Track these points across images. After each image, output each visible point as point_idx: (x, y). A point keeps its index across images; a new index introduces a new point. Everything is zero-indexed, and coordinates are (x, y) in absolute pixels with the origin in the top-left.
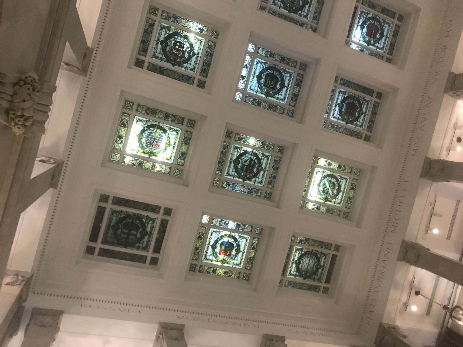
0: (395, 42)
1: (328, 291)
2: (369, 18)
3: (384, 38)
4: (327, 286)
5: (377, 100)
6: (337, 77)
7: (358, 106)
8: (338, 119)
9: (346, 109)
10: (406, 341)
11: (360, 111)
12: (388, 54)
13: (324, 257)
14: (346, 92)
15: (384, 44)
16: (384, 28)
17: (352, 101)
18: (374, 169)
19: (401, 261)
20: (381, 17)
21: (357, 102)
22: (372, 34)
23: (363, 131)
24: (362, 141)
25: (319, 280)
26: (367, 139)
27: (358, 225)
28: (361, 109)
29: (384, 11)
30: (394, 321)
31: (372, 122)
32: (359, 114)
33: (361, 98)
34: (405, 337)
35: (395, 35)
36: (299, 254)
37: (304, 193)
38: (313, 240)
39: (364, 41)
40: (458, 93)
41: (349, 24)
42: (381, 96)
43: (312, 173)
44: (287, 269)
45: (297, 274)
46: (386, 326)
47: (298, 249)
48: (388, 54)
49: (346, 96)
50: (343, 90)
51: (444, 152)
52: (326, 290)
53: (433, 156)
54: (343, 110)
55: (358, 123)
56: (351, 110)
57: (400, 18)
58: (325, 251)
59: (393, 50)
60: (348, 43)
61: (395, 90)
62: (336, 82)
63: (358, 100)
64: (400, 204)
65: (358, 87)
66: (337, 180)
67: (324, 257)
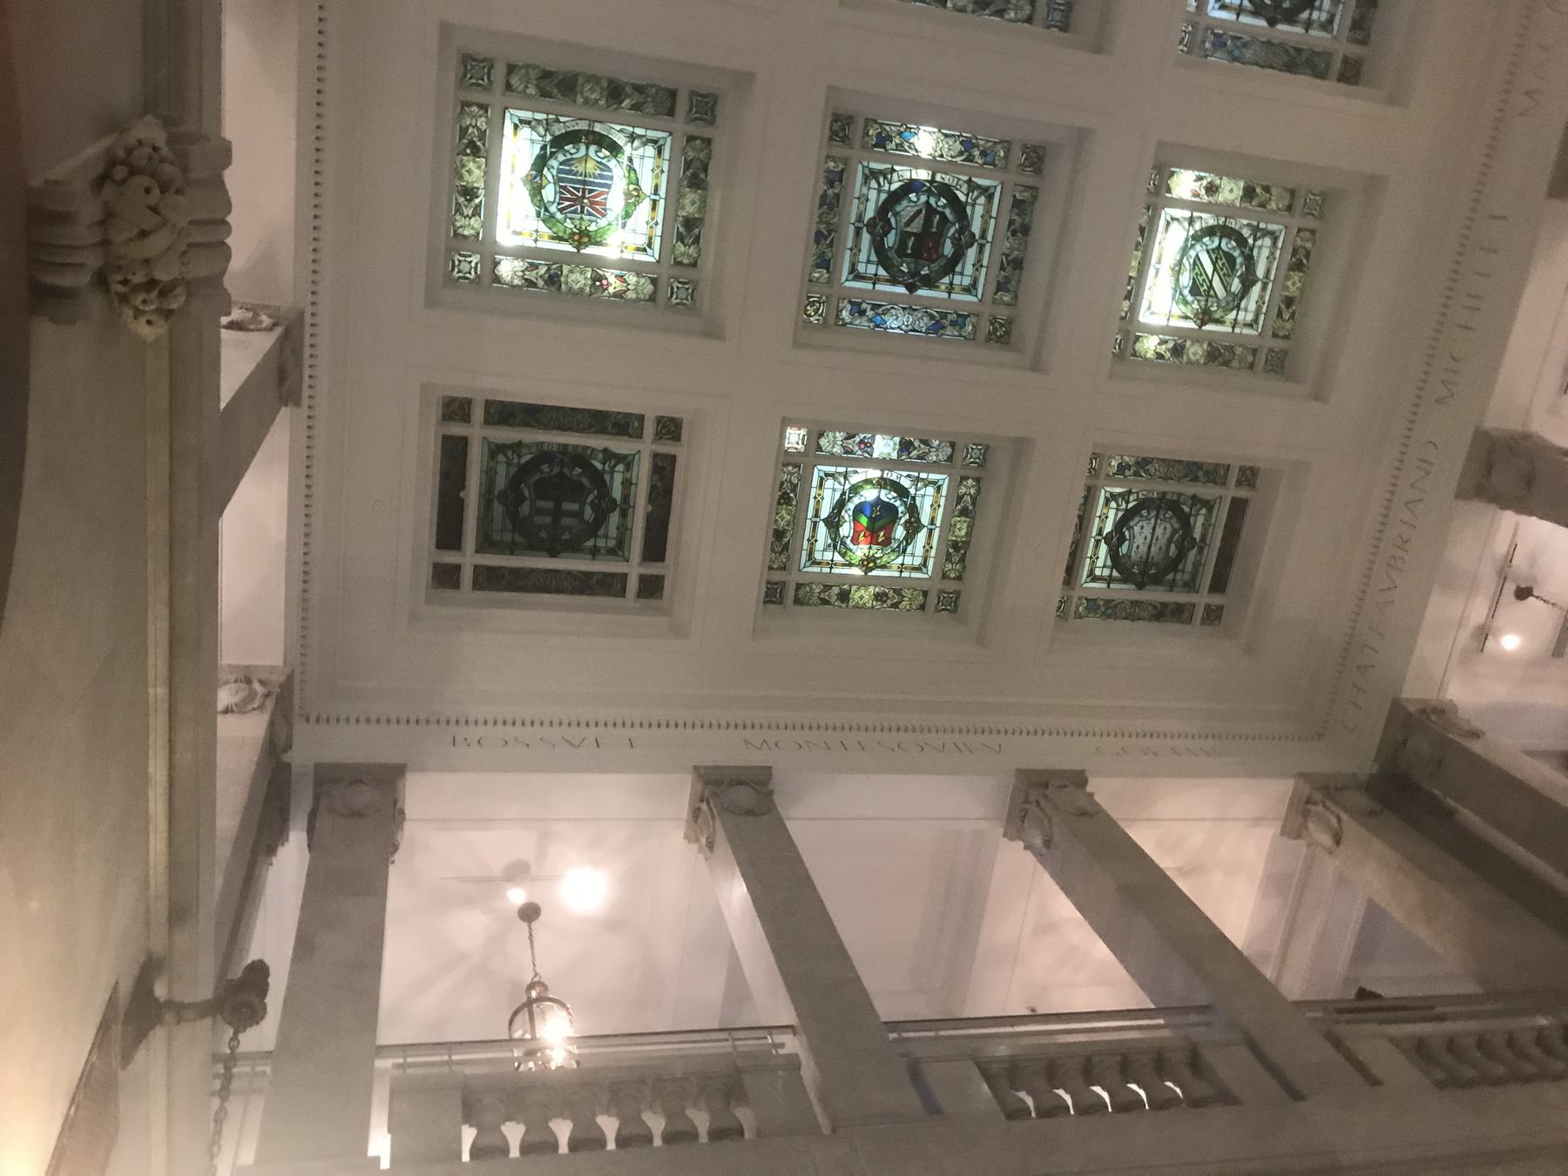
1: (1219, 617)
4: (1216, 600)
10: (1476, 747)
13: (1204, 511)
23: (1333, 41)
30: (1442, 687)
34: (1476, 735)
37: (1126, 304)
44: (1083, 558)
46: (1412, 709)
52: (1213, 615)
58: (1206, 491)
66: (1241, 241)
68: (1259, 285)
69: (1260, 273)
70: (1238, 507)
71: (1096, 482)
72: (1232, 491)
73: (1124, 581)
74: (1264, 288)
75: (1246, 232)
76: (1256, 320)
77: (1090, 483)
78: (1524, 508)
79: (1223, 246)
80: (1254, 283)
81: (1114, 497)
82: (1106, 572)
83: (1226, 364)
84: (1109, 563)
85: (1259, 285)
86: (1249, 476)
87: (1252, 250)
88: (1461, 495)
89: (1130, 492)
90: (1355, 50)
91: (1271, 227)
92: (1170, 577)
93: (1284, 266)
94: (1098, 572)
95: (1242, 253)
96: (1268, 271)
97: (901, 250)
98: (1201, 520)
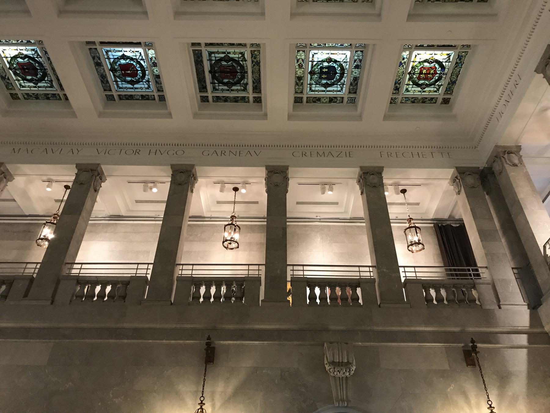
0: (137, 99)
1: (204, 101)
2: (139, 62)
3: (323, 89)
4: (210, 99)
5: (251, 99)
6: (258, 45)
7: (235, 80)
8: (313, 61)
9: (224, 66)
10: (189, 193)
11: (232, 83)
12: (307, 98)
13: (242, 88)
14: (246, 61)
15: (317, 91)
16: (336, 86)
17: (238, 71)
18: (170, 115)
19: (266, 169)
20: (444, 82)
21: (437, 78)
22: (125, 71)
23: (307, 93)
24: (199, 95)
25: (214, 89)
26: (298, 101)
27: (386, 117)
28: (428, 86)
29: (355, 82)
30: (201, 177)
31: (226, 99)
32: (422, 84)
33: (246, 80)
34: (192, 191)
35: (332, 100)
36: (238, 58)
37: (316, 45)
38: (259, 70)
39: (412, 67)
40: (361, 180)
41: (436, 43)
42: (445, 103)
43: (342, 48)
44: (113, 47)
45: (213, 62)
46: (194, 170)
47: (243, 54)
48: (307, 98)
49: (241, 62)
50: (246, 57)
51: (390, 182)
52: (204, 99)
53: (291, 172)
54: (224, 63)
55: (314, 86)
56: (27, 69)
57: (446, 101)
58: (250, 87)
59: (127, 99)
60: (410, 48)
61: (360, 117)
62: (252, 45)
63: (243, 77)
64: (348, 155)
65: (257, 73)
66: (339, 80)
67: (242, 88)
68: (132, 86)
69: (136, 86)
70: (244, 99)
71: (143, 46)
72: (156, 94)
73: (211, 65)
74: (130, 88)
75: (342, 81)
76: (120, 88)
77: (142, 43)
78: (172, 183)
79: (239, 74)
81: (36, 52)
82: (111, 57)
83: (297, 84)
84: (217, 59)
85: (132, 86)
86: (258, 100)
87: (336, 84)
88: (172, 166)
89: (41, 57)
90: (305, 100)
91: (344, 89)
92: (216, 82)
93: (28, 92)
94: (110, 53)
95: (139, 79)
96: (329, 91)
98: (239, 88)
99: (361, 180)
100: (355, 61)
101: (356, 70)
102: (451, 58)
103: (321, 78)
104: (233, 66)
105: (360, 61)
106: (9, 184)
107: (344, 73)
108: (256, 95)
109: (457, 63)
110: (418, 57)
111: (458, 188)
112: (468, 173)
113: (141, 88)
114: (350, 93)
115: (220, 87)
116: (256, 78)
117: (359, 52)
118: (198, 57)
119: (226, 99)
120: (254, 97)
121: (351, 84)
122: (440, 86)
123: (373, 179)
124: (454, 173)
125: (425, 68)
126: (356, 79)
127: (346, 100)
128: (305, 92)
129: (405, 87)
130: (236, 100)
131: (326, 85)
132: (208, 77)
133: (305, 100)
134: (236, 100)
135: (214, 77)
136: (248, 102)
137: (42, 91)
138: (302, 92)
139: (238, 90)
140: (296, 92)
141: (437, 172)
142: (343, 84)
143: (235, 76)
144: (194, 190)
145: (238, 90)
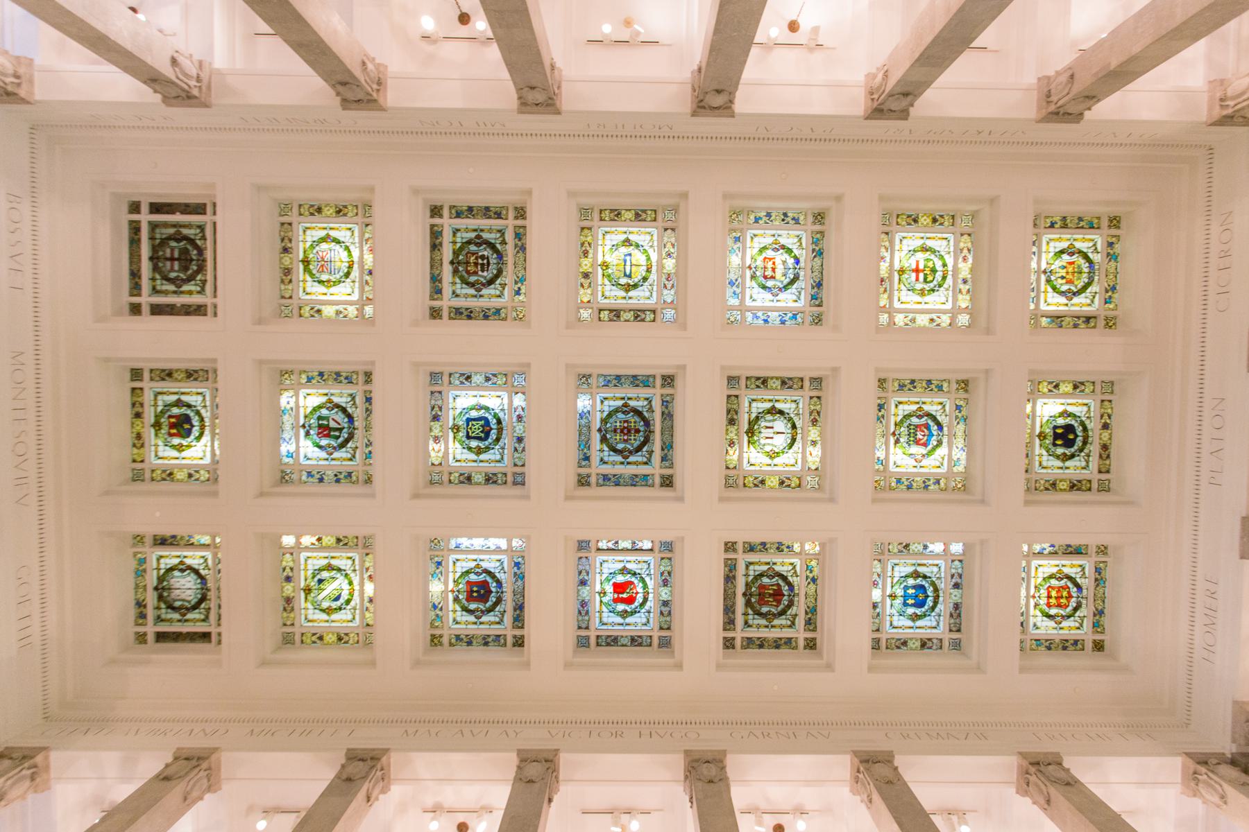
5: (801, 643)
11: (774, 615)
73: (747, 584)
80: (624, 618)
97: (320, 418)
99: (861, 776)
100: (952, 576)
101: (955, 592)
102: (798, 569)
103: (905, 604)
104: (778, 585)
105: (960, 576)
106: (31, 796)
107: (938, 596)
108: (810, 635)
109: (1096, 580)
110: (1040, 569)
111: (1215, 790)
112: (1215, 761)
113: (636, 624)
114: (661, 628)
115: (756, 622)
116: (811, 605)
117: (957, 563)
118: (730, 571)
119: (177, 637)
120: (806, 639)
121: (951, 615)
122: (1082, 618)
123: (710, 771)
124: (1184, 767)
125: (1053, 588)
126: (957, 606)
127: (946, 644)
128: (592, 627)
129: (451, 615)
130: (777, 644)
131: (915, 617)
132: (740, 602)
133: (593, 641)
134: (777, 644)
135: (748, 604)
136: (796, 648)
137: (483, 630)
138: (587, 628)
139: (782, 627)
140: (580, 628)
141: (1154, 762)
142: (649, 612)
143: (779, 602)
144: (556, 798)
145: (782, 627)
